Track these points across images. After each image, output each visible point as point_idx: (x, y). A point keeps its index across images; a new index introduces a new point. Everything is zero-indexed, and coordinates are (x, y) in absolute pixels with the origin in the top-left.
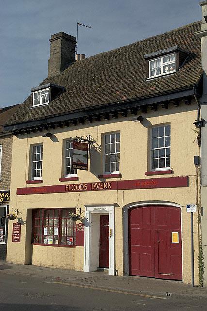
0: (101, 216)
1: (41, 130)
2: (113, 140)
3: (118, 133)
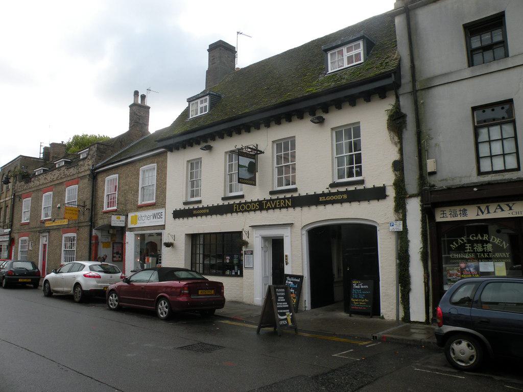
0: (273, 240)
1: (198, 143)
2: (286, 149)
3: (292, 140)
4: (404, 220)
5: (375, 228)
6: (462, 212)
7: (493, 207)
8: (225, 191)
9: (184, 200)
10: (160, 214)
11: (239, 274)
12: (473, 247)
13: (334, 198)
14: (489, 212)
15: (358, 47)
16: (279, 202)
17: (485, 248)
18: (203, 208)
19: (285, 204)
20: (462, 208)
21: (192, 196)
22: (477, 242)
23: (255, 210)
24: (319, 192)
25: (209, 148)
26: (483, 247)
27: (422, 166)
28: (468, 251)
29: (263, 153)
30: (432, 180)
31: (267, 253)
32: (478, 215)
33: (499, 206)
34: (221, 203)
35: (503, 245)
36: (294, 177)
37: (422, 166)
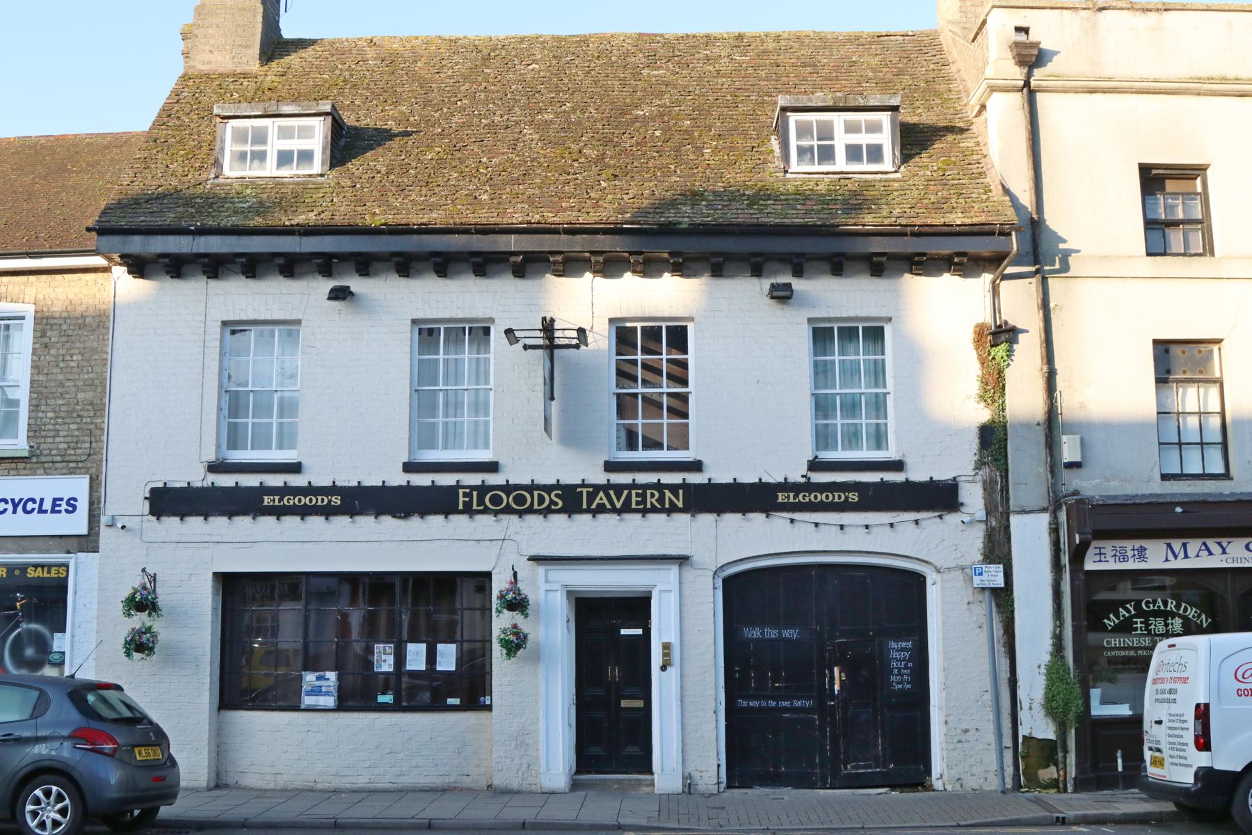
6: (1136, 552)
7: (1194, 545)
8: (218, 446)
9: (212, 457)
12: (1147, 624)
13: (821, 497)
14: (1186, 556)
16: (644, 496)
17: (1170, 627)
18: (310, 490)
19: (661, 500)
20: (1138, 543)
21: (234, 444)
22: (1157, 614)
23: (547, 512)
24: (776, 477)
26: (1166, 625)
28: (1139, 632)
32: (1167, 560)
33: (1204, 544)
34: (398, 479)
35: (1202, 621)
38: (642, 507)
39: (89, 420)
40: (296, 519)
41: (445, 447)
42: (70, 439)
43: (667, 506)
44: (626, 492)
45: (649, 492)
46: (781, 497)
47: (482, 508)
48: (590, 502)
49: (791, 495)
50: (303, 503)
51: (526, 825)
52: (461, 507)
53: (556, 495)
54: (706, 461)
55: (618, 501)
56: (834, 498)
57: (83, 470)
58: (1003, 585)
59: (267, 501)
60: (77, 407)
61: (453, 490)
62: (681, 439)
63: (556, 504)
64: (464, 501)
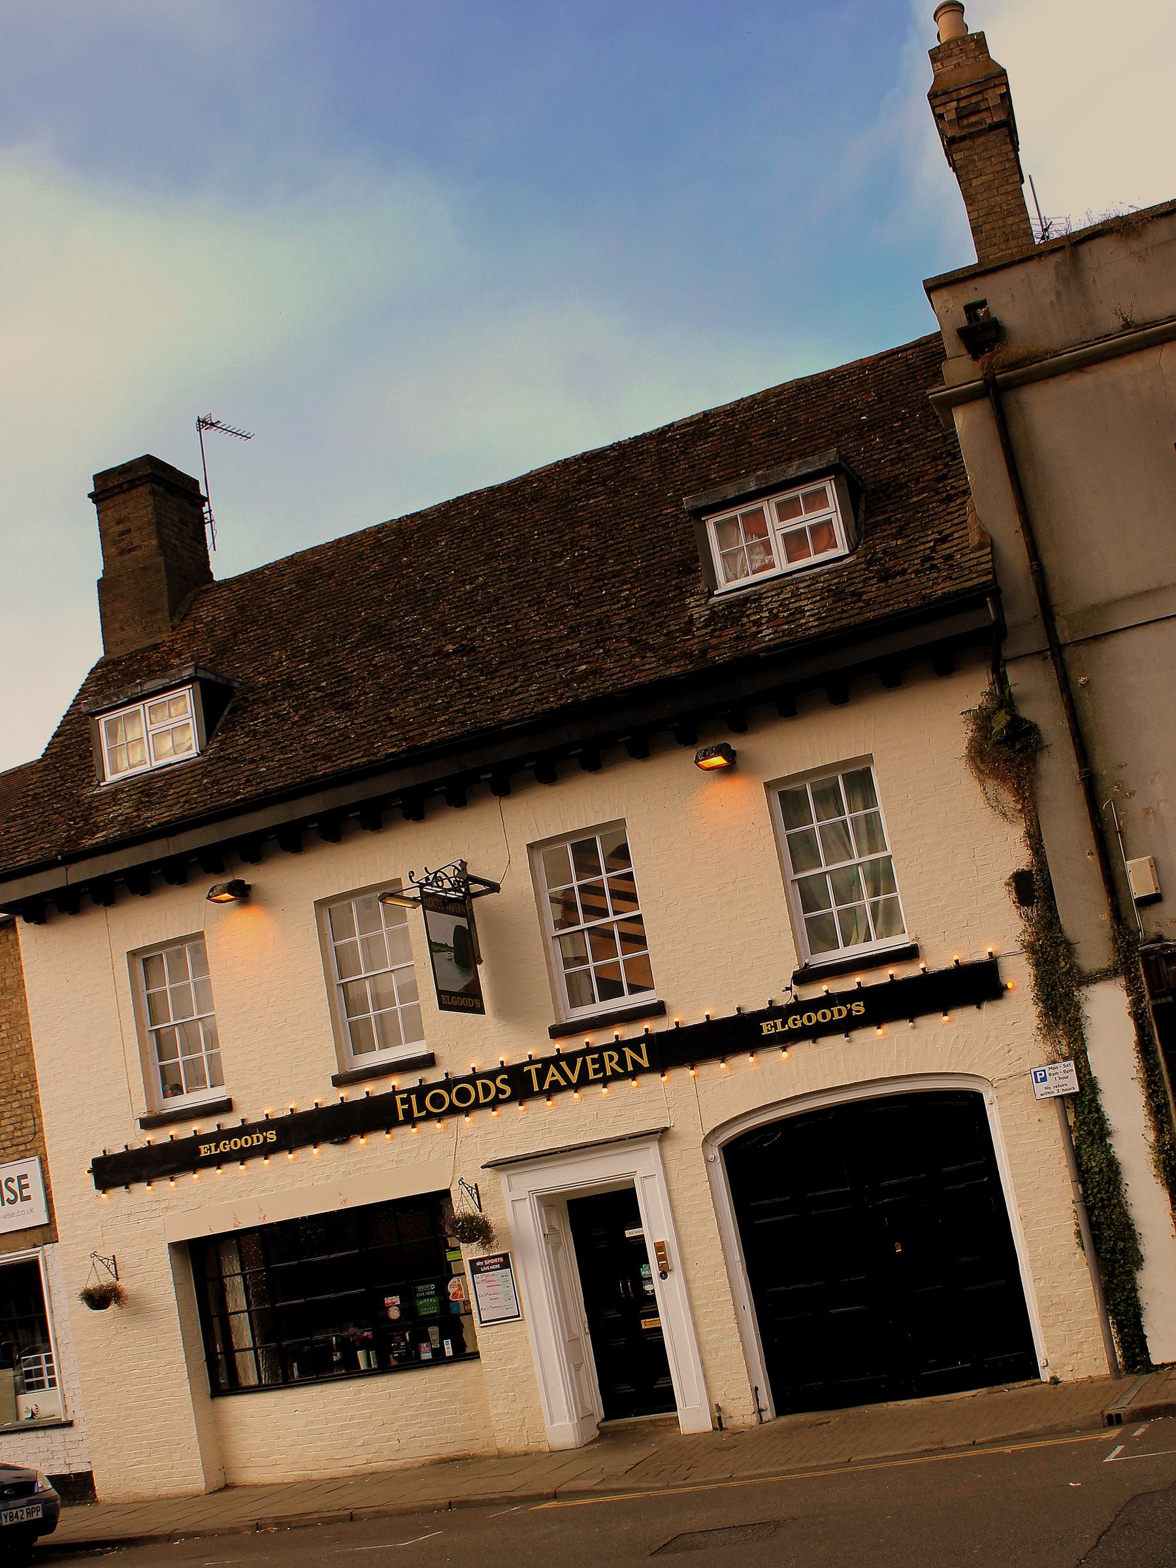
4: (1079, 1056)
5: (977, 1098)
9: (142, 1111)
10: (15, 1186)
11: (449, 1351)
13: (817, 1017)
15: (816, 500)
16: (600, 1061)
18: (246, 1129)
19: (622, 1062)
23: (494, 1104)
24: (756, 1004)
25: (242, 893)
27: (1113, 881)
29: (494, 888)
30: (1148, 924)
31: (561, 1250)
34: (332, 1097)
36: (214, 1060)
37: (1113, 881)
38: (601, 1075)
39: (27, 1094)
40: (840, 1039)
41: (385, 1045)
42: (14, 1119)
43: (630, 1068)
44: (580, 1060)
45: (606, 1055)
46: (766, 1028)
47: (424, 1113)
48: (541, 1082)
49: (779, 1022)
50: (814, 1022)
51: (453, 1505)
52: (401, 1118)
53: (503, 1081)
54: (669, 1001)
55: (573, 1073)
56: (833, 1016)
57: (32, 1152)
58: (1077, 1089)
59: (204, 1150)
60: (15, 1082)
61: (388, 1099)
62: (888, 917)
63: (504, 1092)
64: (403, 1110)
